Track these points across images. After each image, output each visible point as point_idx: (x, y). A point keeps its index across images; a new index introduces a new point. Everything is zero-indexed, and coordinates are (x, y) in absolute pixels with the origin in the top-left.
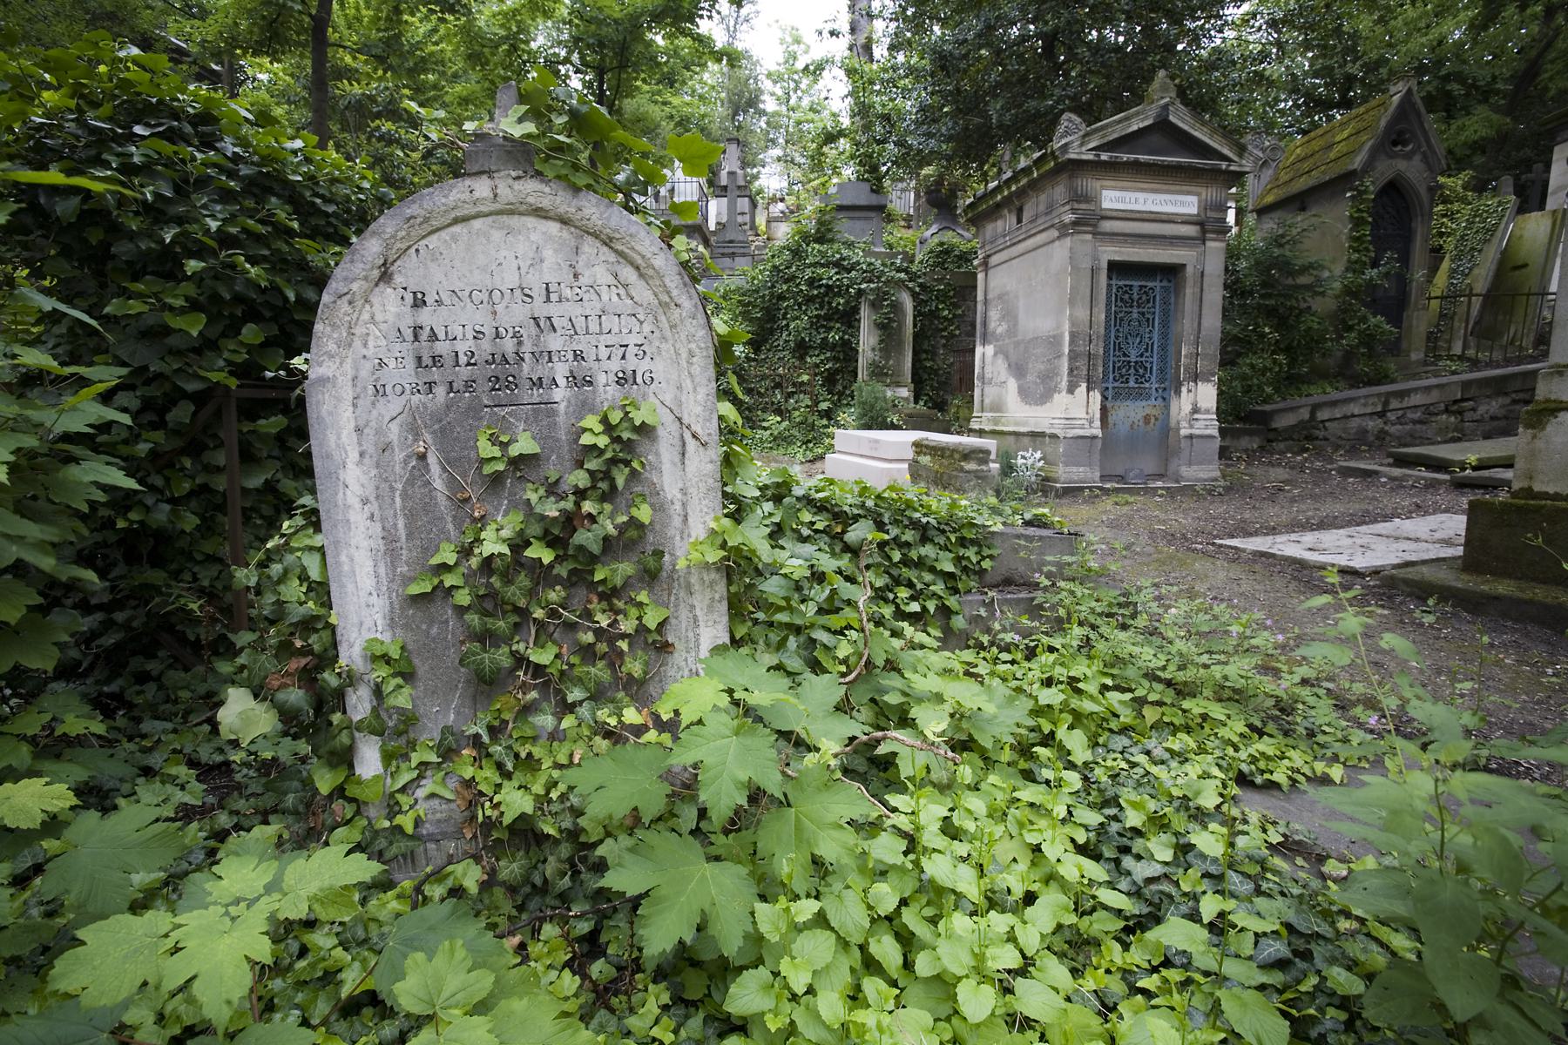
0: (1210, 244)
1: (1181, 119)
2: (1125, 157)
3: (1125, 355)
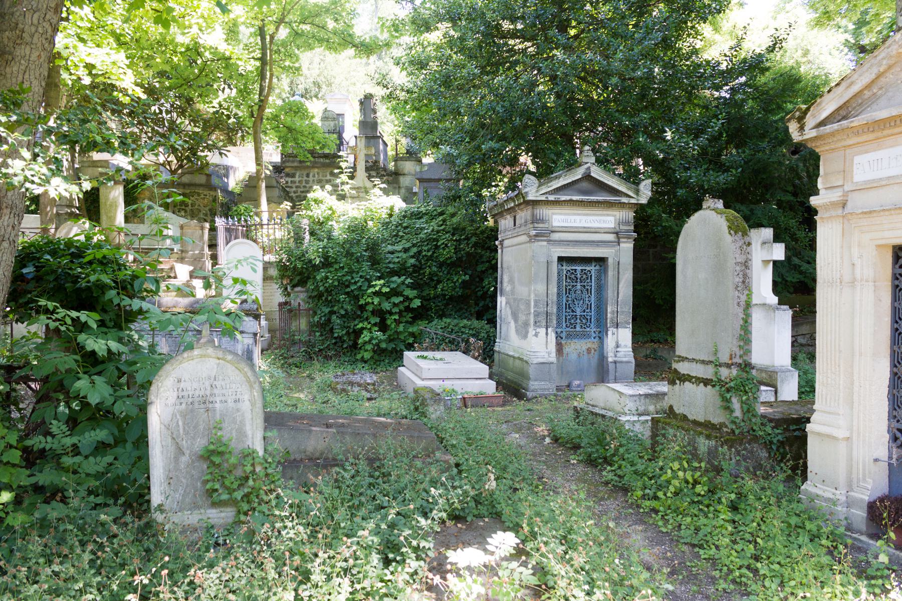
1: (598, 173)
2: (563, 198)
3: (573, 311)
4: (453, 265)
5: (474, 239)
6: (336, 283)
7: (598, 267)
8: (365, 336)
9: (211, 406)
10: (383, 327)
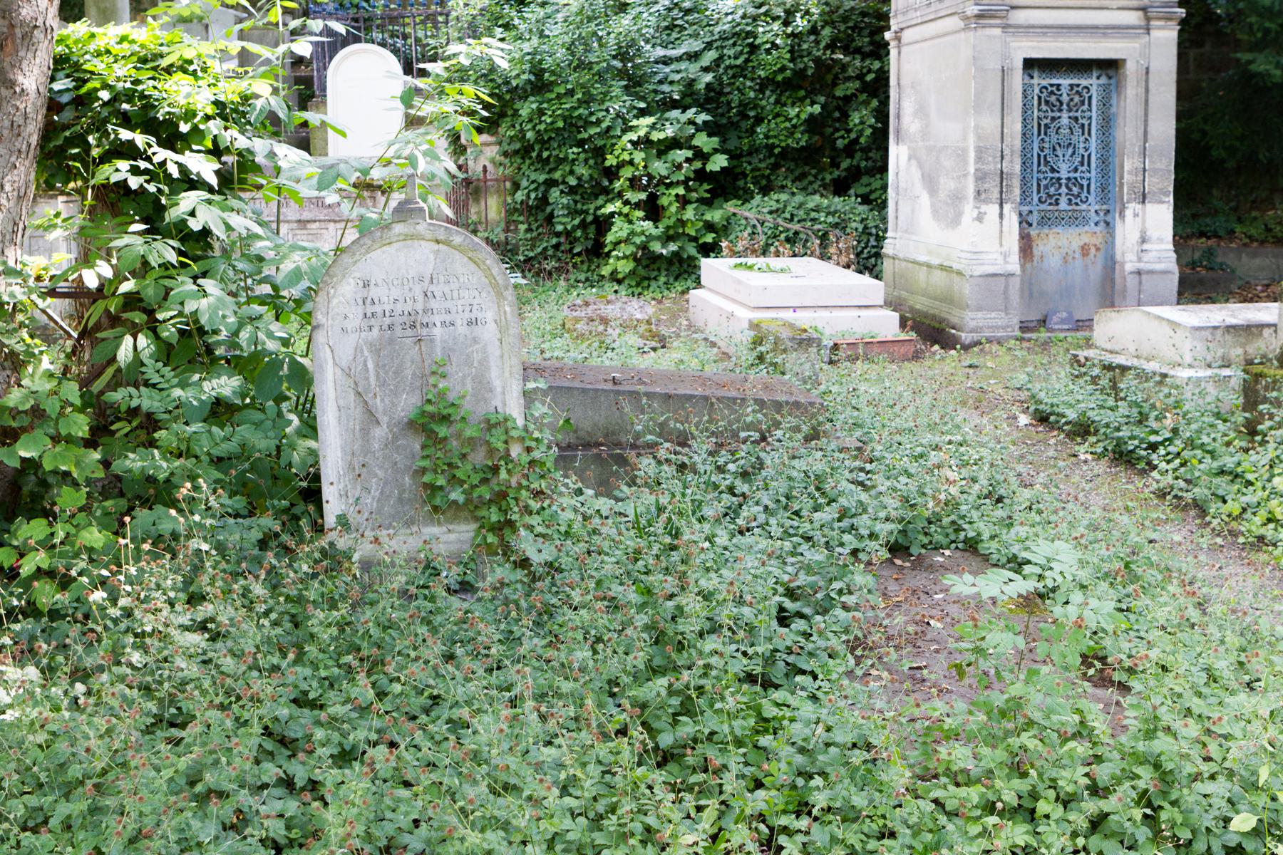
0: (1154, 33)
3: (1053, 170)
4: (788, 85)
5: (827, 32)
6: (560, 124)
7: (1103, 80)
8: (619, 230)
9: (425, 332)
10: (653, 210)
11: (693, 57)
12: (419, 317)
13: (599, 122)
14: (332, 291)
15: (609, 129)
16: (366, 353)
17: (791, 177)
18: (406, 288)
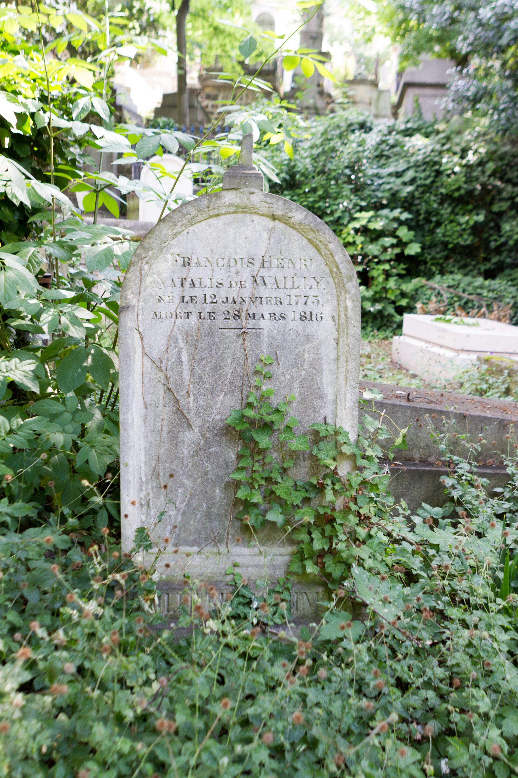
9: (250, 323)
11: (398, 175)
12: (245, 306)
13: (332, 213)
14: (146, 267)
15: (339, 218)
16: (181, 344)
17: (457, 266)
18: (233, 270)
